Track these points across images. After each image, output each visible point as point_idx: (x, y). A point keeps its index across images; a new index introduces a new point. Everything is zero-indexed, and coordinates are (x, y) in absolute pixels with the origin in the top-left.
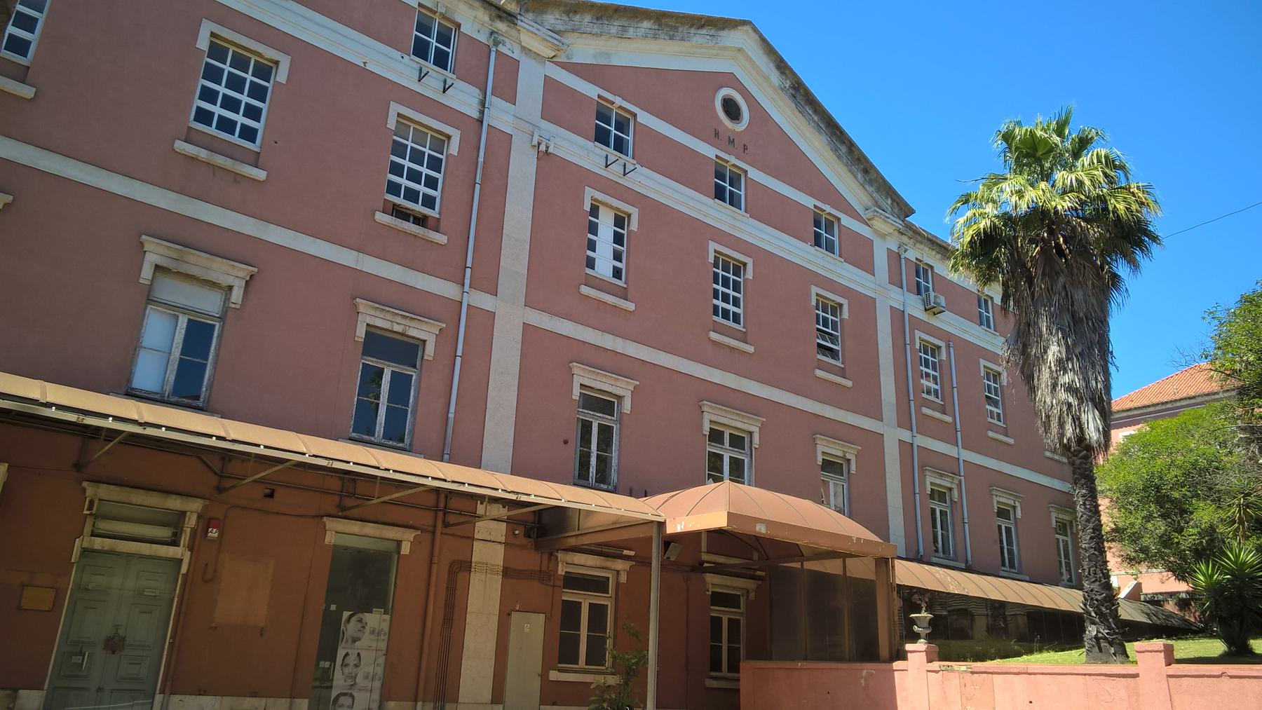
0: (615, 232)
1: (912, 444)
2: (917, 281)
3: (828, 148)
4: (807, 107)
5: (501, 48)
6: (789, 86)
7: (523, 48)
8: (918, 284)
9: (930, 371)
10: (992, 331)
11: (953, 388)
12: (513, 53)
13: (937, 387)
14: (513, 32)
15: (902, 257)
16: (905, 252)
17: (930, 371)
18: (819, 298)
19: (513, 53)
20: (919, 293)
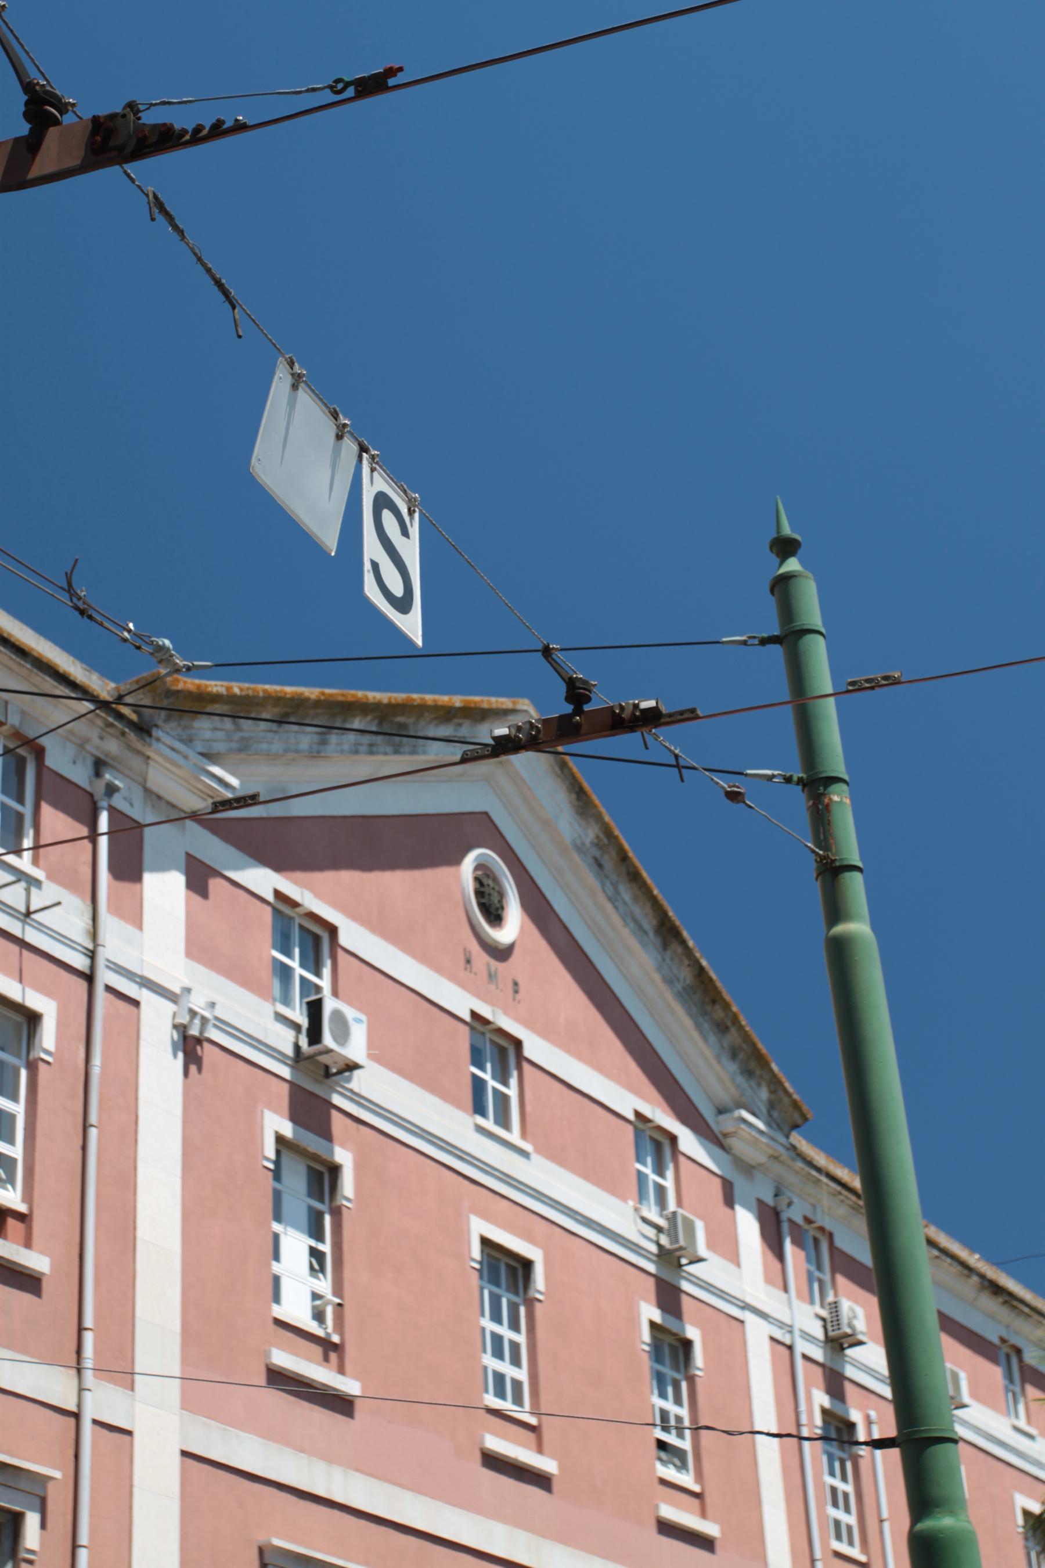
0: (310, 1209)
1: (77, 1416)
2: (476, 1079)
3: (657, 977)
4: (622, 888)
5: (118, 801)
6: (592, 843)
7: (148, 792)
8: (478, 1085)
9: (504, 1331)
10: (514, 1136)
11: (881, 1521)
12: (132, 805)
13: (522, 1374)
14: (136, 762)
15: (784, 1216)
16: (790, 1204)
17: (504, 1331)
18: (661, 1336)
19: (132, 805)
20: (479, 1108)
